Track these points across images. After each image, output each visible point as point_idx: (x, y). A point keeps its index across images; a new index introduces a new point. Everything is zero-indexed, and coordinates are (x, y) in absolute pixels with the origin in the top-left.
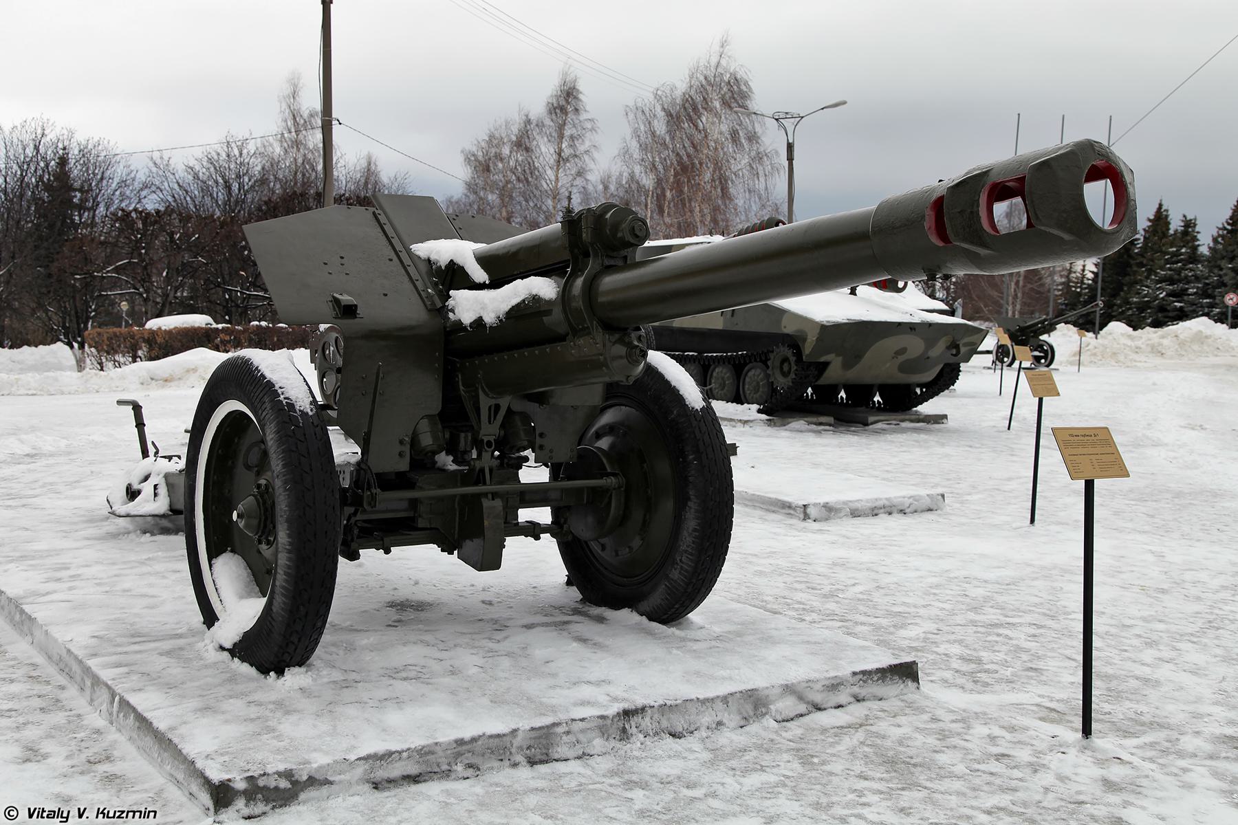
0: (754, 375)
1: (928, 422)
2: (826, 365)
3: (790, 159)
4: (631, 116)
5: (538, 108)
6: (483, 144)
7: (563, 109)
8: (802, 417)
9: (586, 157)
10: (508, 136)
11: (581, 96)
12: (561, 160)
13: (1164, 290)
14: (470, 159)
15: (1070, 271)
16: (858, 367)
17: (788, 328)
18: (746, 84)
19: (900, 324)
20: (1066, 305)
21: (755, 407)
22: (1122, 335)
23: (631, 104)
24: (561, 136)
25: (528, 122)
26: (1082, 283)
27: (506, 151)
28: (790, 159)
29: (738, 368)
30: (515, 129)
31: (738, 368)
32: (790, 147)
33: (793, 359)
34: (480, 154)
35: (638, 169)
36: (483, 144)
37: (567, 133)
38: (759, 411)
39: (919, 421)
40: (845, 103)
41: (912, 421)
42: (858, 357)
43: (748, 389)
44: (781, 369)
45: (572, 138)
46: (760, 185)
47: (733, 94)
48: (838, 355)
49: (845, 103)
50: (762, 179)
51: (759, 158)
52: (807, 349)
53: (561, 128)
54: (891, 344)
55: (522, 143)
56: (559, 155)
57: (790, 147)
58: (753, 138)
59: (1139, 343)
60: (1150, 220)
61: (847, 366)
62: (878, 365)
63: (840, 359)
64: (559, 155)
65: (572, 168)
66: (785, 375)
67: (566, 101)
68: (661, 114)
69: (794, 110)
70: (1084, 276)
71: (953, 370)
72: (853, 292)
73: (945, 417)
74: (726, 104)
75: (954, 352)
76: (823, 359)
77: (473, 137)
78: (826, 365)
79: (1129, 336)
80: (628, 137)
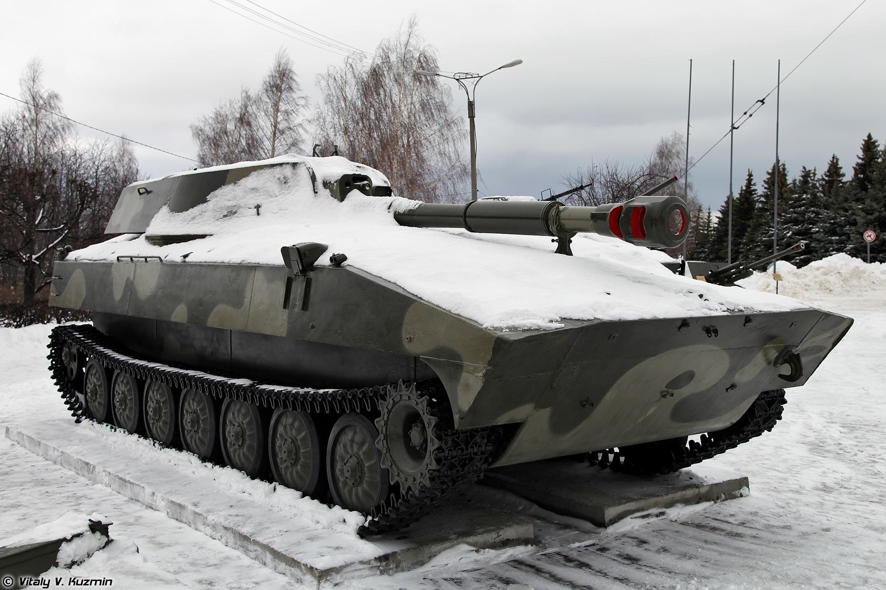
0: (349, 443)
1: (716, 499)
2: (513, 429)
3: (472, 116)
4: (324, 83)
5: (256, 86)
6: (210, 121)
7: (278, 88)
8: (463, 535)
9: (301, 130)
10: (232, 113)
11: (295, 77)
12: (276, 131)
13: (789, 229)
14: (198, 133)
15: (698, 218)
16: (583, 427)
17: (417, 342)
18: (434, 61)
19: (684, 323)
20: (697, 244)
21: (355, 519)
22: (789, 273)
23: (324, 72)
24: (277, 110)
25: (248, 98)
26: (709, 226)
27: (230, 126)
28: (472, 116)
29: (322, 420)
30: (237, 106)
31: (322, 420)
32: (471, 105)
33: (430, 420)
34: (207, 128)
35: (331, 133)
36: (210, 121)
37: (283, 107)
38: (363, 533)
39: (698, 499)
40: (520, 62)
41: (687, 502)
42: (587, 404)
43: (343, 471)
44: (407, 439)
45: (287, 112)
46: (450, 149)
47: (424, 72)
48: (540, 406)
49: (520, 62)
50: (451, 144)
51: (448, 124)
52: (464, 394)
53: (276, 106)
54: (662, 366)
55: (244, 120)
56: (275, 127)
57: (471, 105)
58: (442, 107)
59: (807, 280)
60: (769, 173)
61: (559, 426)
62: (627, 412)
63: (546, 413)
64: (275, 127)
65: (288, 138)
66: (417, 454)
67: (281, 83)
68: (352, 82)
69: (474, 71)
70: (709, 221)
71: (770, 403)
72: (564, 248)
73: (744, 482)
74: (417, 77)
75: (786, 369)
76: (503, 419)
77: (203, 112)
78: (513, 429)
79: (795, 274)
80: (321, 102)
